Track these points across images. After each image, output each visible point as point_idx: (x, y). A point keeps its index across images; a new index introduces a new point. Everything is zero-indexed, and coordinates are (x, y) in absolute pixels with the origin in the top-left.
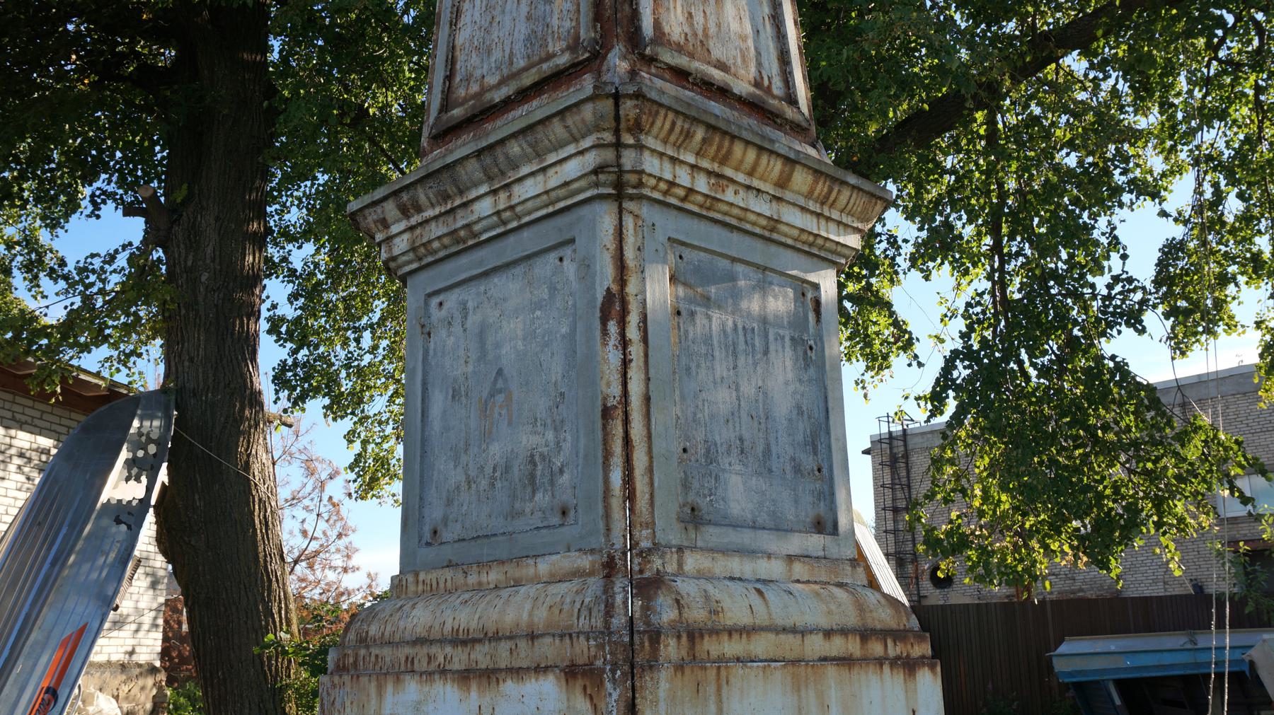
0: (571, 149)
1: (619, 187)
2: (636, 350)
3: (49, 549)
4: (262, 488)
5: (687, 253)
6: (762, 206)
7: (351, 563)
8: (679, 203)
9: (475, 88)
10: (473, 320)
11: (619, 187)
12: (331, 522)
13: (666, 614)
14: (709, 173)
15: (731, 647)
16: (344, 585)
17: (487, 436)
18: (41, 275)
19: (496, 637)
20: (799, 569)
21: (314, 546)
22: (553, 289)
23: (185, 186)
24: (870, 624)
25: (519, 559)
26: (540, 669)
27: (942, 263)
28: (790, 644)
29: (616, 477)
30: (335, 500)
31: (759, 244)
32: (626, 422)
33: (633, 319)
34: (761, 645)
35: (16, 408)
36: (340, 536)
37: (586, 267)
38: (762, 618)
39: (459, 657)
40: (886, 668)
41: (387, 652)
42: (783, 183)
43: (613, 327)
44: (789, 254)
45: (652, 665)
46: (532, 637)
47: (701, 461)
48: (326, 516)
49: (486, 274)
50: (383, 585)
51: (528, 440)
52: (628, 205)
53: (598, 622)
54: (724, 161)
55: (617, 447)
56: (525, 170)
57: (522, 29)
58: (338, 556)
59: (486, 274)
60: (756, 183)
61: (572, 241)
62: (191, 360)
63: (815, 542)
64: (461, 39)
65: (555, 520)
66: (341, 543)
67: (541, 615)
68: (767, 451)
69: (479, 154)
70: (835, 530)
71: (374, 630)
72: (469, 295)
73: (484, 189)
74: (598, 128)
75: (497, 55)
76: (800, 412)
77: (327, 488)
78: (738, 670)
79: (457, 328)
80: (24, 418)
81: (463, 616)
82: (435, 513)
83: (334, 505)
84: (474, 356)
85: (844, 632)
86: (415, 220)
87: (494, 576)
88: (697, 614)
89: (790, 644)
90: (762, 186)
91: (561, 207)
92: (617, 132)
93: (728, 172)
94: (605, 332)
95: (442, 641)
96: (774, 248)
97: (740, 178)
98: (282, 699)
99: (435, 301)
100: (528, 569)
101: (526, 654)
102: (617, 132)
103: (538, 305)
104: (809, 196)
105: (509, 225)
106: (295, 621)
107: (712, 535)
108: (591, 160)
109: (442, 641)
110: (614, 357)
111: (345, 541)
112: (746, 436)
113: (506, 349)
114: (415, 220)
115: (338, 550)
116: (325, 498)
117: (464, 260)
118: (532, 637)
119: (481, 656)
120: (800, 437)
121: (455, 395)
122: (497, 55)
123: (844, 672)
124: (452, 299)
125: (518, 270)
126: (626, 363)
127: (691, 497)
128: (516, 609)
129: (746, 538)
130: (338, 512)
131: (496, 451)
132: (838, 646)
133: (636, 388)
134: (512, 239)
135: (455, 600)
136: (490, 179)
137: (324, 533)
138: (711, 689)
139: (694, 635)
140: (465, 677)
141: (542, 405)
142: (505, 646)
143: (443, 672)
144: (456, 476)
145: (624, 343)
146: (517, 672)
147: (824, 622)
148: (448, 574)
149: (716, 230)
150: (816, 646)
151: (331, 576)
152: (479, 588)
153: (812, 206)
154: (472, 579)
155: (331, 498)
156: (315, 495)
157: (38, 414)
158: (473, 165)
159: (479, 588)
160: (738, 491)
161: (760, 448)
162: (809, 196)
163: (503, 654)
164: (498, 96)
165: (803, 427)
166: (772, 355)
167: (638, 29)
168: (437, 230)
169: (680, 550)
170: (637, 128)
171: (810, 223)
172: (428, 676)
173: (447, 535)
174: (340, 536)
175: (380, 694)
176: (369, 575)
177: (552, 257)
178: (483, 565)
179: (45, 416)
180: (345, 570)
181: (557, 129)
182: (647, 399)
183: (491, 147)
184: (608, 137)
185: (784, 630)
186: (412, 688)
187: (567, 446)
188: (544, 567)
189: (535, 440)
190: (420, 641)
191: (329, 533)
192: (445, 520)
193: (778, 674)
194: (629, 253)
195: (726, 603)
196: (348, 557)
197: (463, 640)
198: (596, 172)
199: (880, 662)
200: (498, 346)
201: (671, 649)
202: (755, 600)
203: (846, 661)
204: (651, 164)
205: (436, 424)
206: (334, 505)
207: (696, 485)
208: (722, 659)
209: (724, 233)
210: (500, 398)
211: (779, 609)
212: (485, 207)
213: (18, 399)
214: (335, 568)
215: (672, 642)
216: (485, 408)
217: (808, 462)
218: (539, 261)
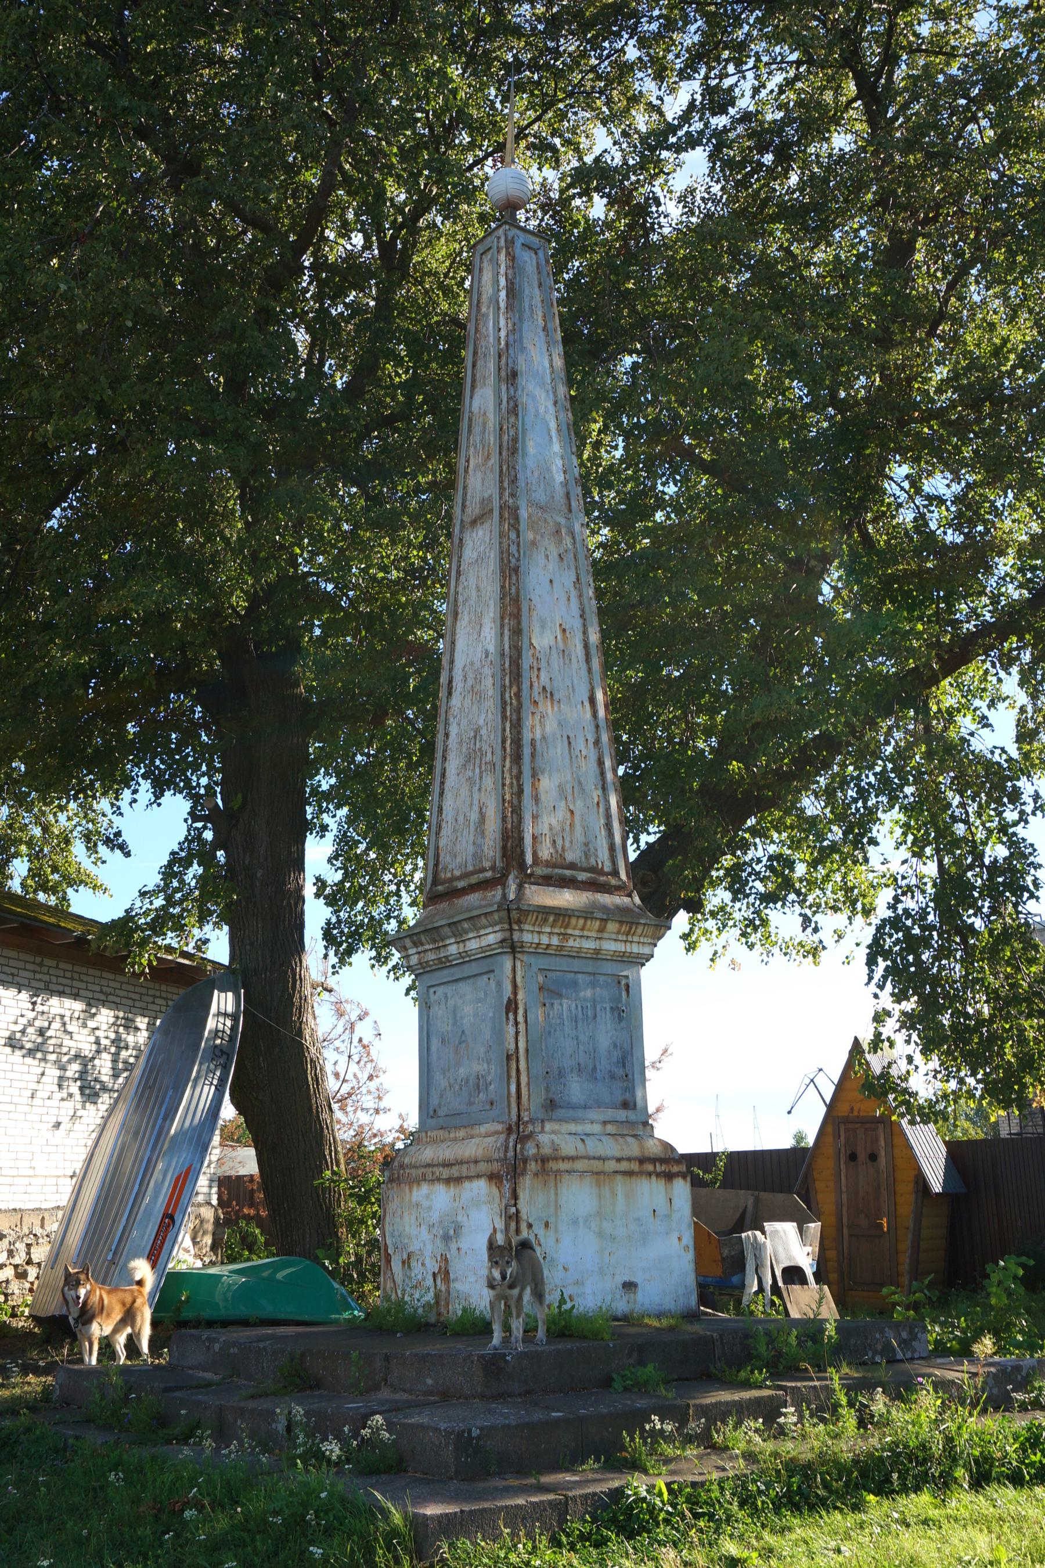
0: (490, 930)
1: (513, 948)
2: (522, 1027)
3: (160, 1107)
4: (313, 1050)
5: (549, 974)
6: (590, 945)
7: (382, 1105)
8: (541, 951)
9: (449, 875)
10: (451, 1003)
11: (513, 948)
12: (362, 1063)
13: (531, 1150)
14: (559, 934)
15: (563, 1166)
16: (376, 1127)
17: (458, 1064)
18: (99, 843)
19: (461, 1163)
20: (610, 1128)
21: (345, 1089)
22: (486, 993)
23: (240, 796)
24: (647, 1155)
25: (472, 1126)
26: (479, 1176)
27: (865, 853)
28: (597, 1165)
29: (513, 1088)
30: (365, 1042)
31: (591, 962)
32: (518, 1061)
33: (521, 1012)
34: (580, 1165)
35: (104, 982)
36: (371, 1078)
37: (499, 984)
38: (582, 1150)
39: (446, 1173)
40: (654, 1178)
41: (413, 1172)
42: (601, 930)
43: (511, 1016)
44: (609, 963)
45: (523, 1173)
46: (476, 1162)
47: (556, 1076)
48: (356, 1058)
49: (456, 981)
50: (413, 1122)
51: (477, 1067)
52: (518, 955)
53: (502, 1155)
54: (567, 927)
55: (514, 1073)
56: (471, 935)
57: (471, 850)
58: (370, 1097)
59: (456, 981)
60: (586, 933)
61: (493, 971)
62: (252, 944)
63: (622, 1115)
64: (442, 843)
65: (488, 1107)
66: (372, 1085)
67: (480, 1153)
68: (595, 1068)
69: (449, 925)
70: (634, 1107)
71: (407, 1161)
72: (449, 989)
73: (452, 940)
74: (501, 922)
75: (459, 860)
76: (615, 1045)
77: (357, 1028)
78: (566, 1177)
79: (443, 1006)
80: (109, 990)
81: (446, 1152)
82: (435, 1101)
83: (364, 1047)
84: (451, 1022)
85: (629, 1159)
86: (420, 949)
87: (461, 1133)
88: (547, 1150)
89: (597, 1165)
90: (589, 934)
91: (487, 955)
92: (510, 924)
93: (569, 931)
94: (508, 1019)
95: (438, 1165)
96: (600, 962)
97: (577, 932)
98: (335, 1226)
99: (432, 990)
100: (477, 1131)
101: (473, 1170)
102: (510, 924)
103: (479, 1001)
104: (618, 933)
105: (466, 960)
106: (342, 1161)
107: (560, 1113)
108: (499, 936)
109: (438, 1165)
110: (511, 1030)
111: (376, 1082)
112: (582, 1062)
113: (465, 1021)
114: (420, 949)
115: (369, 1092)
116: (355, 1040)
117: (445, 972)
118: (476, 1162)
119: (455, 1171)
120: (615, 1059)
121: (443, 1041)
122: (459, 860)
123: (627, 1179)
124: (440, 990)
125: (470, 981)
126: (517, 1033)
127: (550, 1095)
128: (470, 1149)
129: (580, 1113)
130: (368, 1054)
131: (462, 1071)
132: (624, 1166)
133: (522, 1045)
134: (467, 966)
135: (444, 1145)
136: (455, 936)
137: (355, 1075)
138: (552, 1184)
139: (544, 1160)
140: (448, 1181)
141: (482, 1050)
142: (465, 1166)
143: (439, 1179)
144: (444, 1083)
145: (516, 1023)
146: (469, 1178)
147: (618, 1155)
148: (441, 1133)
149: (565, 960)
150: (611, 1165)
151: (364, 1118)
152: (455, 1139)
153: (620, 937)
154: (452, 1135)
155: (360, 1040)
156: (346, 1036)
157: (118, 985)
158: (447, 930)
159: (455, 1139)
160: (576, 1089)
161: (590, 1067)
162: (618, 933)
163: (464, 1170)
164: (460, 884)
165: (616, 1055)
166: (598, 1018)
167: (524, 861)
168: (431, 956)
169: (543, 1121)
170: (519, 922)
171: (620, 947)
172: (432, 1181)
173: (441, 1113)
174: (371, 1078)
175: (411, 1191)
176: (400, 1116)
177: (485, 977)
178: (457, 1128)
179: (124, 987)
180: (377, 1111)
181: (484, 921)
182: (527, 1050)
183: (455, 923)
184: (506, 926)
185: (594, 1158)
186: (425, 1188)
187: (493, 1071)
188: (483, 1129)
189: (479, 1067)
190: (428, 1165)
191: (359, 1075)
192: (440, 1105)
193: (588, 1179)
194: (519, 979)
195: (563, 1146)
196: (380, 1098)
197: (447, 1165)
198: (502, 942)
199: (650, 1174)
200: (462, 1018)
201: (532, 1166)
202: (580, 1144)
203: (629, 1174)
204: (527, 937)
205: (434, 1056)
206: (364, 1047)
207: (553, 1089)
208: (559, 1171)
209: (570, 960)
210: (464, 1045)
211: (593, 1147)
212: (453, 949)
213: (105, 974)
214: (367, 1110)
215: (533, 1163)
216: (457, 1050)
217: (620, 1072)
218: (479, 978)
